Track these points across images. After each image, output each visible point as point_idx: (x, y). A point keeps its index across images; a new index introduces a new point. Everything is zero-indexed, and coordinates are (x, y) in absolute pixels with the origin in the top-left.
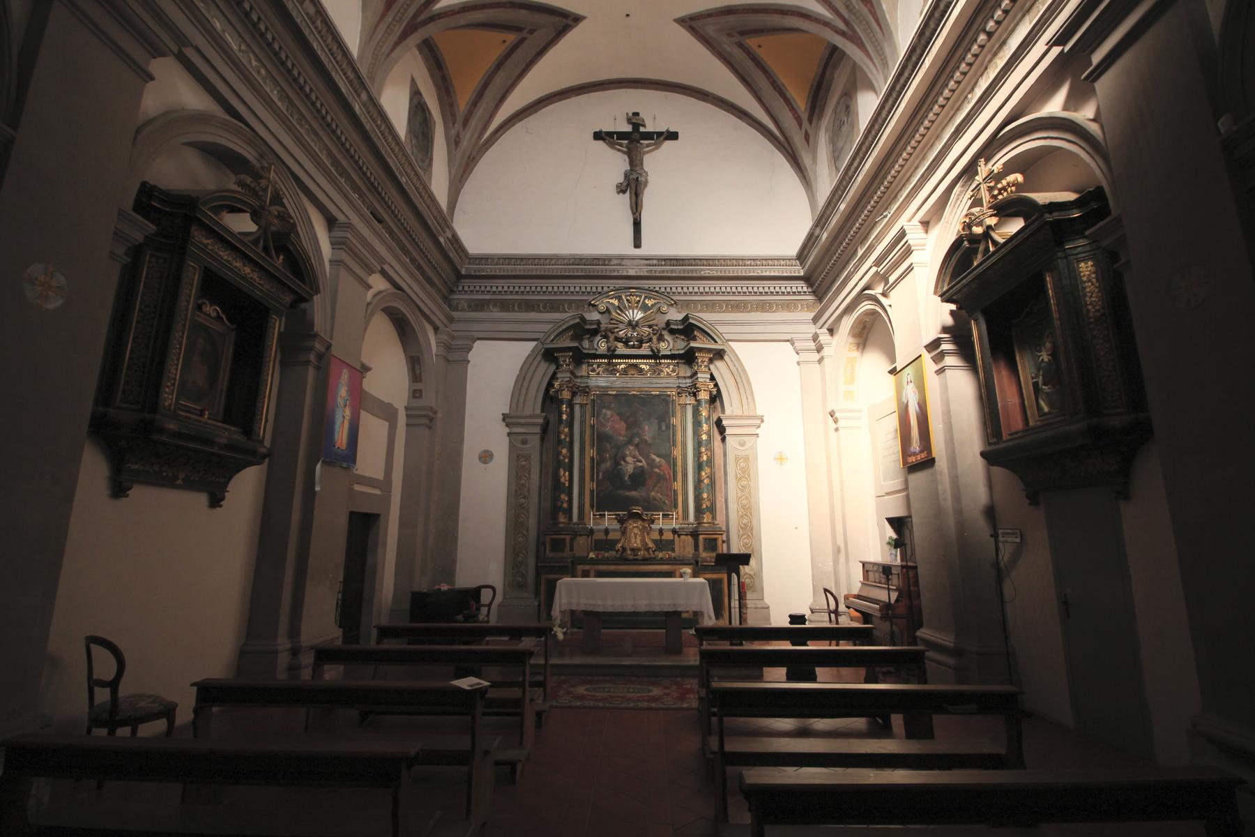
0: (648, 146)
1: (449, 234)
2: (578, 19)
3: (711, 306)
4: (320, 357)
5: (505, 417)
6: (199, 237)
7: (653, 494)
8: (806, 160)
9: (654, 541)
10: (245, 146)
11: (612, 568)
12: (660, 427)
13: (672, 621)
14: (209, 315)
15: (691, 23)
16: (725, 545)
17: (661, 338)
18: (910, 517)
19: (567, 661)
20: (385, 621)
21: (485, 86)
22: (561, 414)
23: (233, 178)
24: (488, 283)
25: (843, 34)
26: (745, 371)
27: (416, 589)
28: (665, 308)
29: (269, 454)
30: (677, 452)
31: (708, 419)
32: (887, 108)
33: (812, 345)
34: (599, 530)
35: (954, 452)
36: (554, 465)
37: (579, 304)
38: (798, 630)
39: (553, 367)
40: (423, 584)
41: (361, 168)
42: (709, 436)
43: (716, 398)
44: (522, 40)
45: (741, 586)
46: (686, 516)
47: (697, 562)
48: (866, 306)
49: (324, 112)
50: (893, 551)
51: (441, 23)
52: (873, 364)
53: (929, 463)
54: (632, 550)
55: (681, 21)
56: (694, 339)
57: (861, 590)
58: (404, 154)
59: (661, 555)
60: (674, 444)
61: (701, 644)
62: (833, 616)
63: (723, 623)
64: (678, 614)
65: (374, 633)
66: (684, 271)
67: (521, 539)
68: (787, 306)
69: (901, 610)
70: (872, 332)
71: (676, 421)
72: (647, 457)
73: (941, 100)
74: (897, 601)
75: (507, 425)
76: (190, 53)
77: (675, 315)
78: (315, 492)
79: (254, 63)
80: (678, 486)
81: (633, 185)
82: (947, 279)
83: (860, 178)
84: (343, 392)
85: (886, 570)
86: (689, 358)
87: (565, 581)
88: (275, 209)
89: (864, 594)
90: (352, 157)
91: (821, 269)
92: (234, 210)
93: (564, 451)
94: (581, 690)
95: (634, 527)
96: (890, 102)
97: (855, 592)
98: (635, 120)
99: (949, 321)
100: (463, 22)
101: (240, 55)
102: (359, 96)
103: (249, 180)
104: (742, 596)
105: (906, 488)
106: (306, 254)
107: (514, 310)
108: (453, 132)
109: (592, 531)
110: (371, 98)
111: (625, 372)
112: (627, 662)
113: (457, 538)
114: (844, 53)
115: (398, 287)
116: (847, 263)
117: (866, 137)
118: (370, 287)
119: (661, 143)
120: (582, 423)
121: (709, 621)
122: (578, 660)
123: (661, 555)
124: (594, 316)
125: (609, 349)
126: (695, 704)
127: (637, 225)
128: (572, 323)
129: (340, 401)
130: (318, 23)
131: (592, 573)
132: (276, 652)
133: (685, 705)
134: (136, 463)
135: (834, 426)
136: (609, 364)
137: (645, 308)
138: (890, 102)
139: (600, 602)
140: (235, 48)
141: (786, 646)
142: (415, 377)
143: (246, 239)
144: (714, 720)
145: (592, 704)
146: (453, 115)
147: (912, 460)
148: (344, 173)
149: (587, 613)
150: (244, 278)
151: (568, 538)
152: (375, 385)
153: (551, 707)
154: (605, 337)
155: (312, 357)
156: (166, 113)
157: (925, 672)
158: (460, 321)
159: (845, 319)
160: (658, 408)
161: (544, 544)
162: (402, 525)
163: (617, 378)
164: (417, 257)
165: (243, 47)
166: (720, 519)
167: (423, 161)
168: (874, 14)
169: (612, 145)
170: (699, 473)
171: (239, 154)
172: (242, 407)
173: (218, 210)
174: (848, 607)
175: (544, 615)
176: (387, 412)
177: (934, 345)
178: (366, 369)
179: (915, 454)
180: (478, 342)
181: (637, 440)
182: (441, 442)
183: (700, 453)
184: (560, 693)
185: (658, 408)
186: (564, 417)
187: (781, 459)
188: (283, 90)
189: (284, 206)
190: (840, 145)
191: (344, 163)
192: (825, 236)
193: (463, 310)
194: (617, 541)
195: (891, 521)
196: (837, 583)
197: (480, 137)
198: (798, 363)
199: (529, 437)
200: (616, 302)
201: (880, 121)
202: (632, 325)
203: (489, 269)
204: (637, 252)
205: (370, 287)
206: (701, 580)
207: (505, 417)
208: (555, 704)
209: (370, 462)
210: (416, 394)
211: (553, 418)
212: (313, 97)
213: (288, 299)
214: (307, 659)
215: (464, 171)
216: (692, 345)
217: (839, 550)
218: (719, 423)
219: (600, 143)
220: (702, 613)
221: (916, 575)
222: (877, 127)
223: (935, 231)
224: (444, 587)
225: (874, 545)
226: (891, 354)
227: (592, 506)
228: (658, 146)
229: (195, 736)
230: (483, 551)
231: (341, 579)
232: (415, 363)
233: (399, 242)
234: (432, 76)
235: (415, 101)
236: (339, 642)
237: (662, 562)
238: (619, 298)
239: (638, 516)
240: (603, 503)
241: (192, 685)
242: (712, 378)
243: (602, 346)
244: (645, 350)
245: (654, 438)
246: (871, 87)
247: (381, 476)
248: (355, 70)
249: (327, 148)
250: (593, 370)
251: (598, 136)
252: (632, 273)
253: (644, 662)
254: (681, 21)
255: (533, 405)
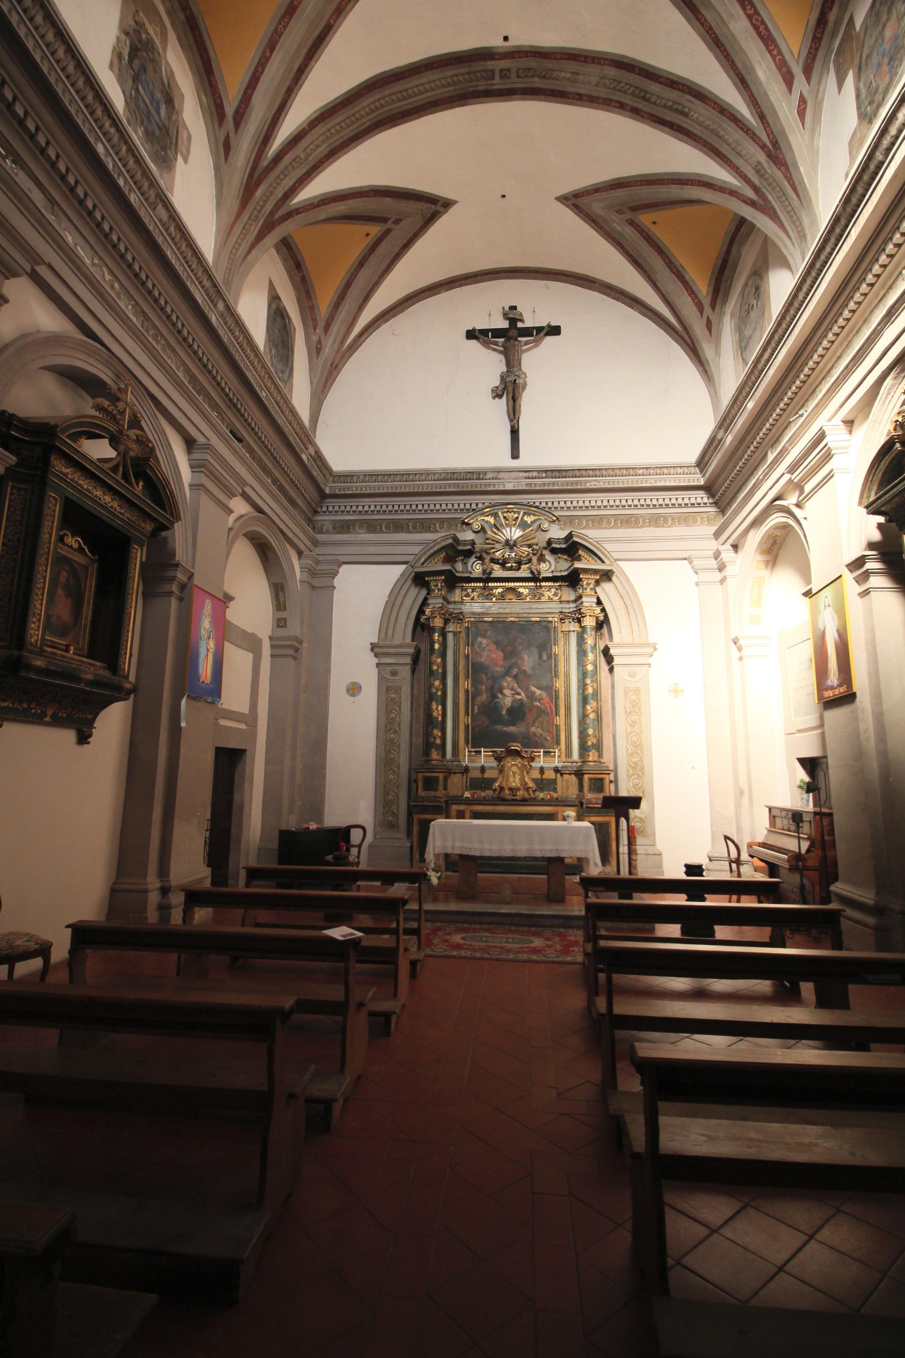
0: (526, 343)
1: (312, 451)
2: (448, 204)
3: (598, 522)
4: (183, 587)
5: (373, 647)
6: (59, 466)
7: (533, 729)
8: (708, 351)
9: (534, 780)
10: (100, 367)
11: (489, 808)
12: (540, 656)
13: (555, 866)
14: (71, 547)
15: (576, 201)
16: (612, 786)
17: (542, 559)
18: (826, 757)
19: (441, 907)
20: (253, 862)
21: (348, 285)
22: (432, 645)
23: (90, 401)
24: (353, 502)
25: (752, 204)
26: (635, 594)
27: (282, 828)
28: (546, 525)
29: (134, 690)
30: (559, 684)
31: (594, 647)
32: (805, 289)
33: (713, 563)
34: (475, 768)
35: (874, 640)
36: (427, 700)
37: (451, 522)
38: (695, 883)
39: (424, 592)
40: (292, 823)
41: (219, 384)
42: (596, 666)
43: (602, 624)
44: (389, 231)
45: (631, 831)
46: (569, 753)
47: (582, 804)
48: (777, 519)
49: (180, 325)
50: (805, 796)
51: (299, 218)
52: (784, 583)
53: (849, 698)
54: (511, 789)
55: (564, 199)
56: (579, 559)
57: (766, 837)
58: (264, 367)
59: (541, 795)
60: (556, 676)
61: (587, 896)
62: (734, 866)
63: (610, 871)
64: (560, 860)
65: (243, 874)
66: (567, 483)
67: (391, 777)
68: (685, 520)
69: (812, 862)
70: (782, 547)
71: (557, 650)
72: (527, 690)
73: (870, 278)
74: (808, 851)
75: (376, 656)
76: (43, 271)
77: (557, 533)
78: (180, 729)
79: (108, 277)
80: (560, 721)
81: (510, 389)
82: (875, 488)
83: (771, 372)
84: (206, 624)
85: (797, 817)
86: (573, 580)
87: (439, 824)
88: (133, 433)
89: (770, 842)
90: (210, 372)
91: (724, 478)
92: (92, 436)
93: (437, 683)
94: (457, 938)
95: (513, 765)
96: (809, 282)
97: (760, 839)
98: (512, 315)
99: (876, 536)
100: (323, 217)
101: (93, 269)
102: (215, 306)
103: (106, 403)
104: (631, 842)
105: (822, 725)
106: (166, 479)
107: (381, 531)
108: (315, 338)
109: (466, 770)
110: (228, 307)
111: (502, 597)
112: (505, 909)
113: (325, 774)
114: (753, 226)
115: (259, 510)
116: (756, 469)
117: (779, 324)
118: (231, 512)
119: (542, 339)
120: (456, 652)
121: (595, 869)
122: (453, 907)
123: (541, 795)
124: (468, 536)
125: (484, 572)
126: (580, 958)
127: (515, 433)
128: (444, 544)
129: (203, 633)
130: (172, 229)
131: (468, 814)
132: (146, 891)
133: (569, 959)
134: (5, 701)
135: (738, 654)
136: (484, 588)
137: (524, 525)
138: (809, 282)
139: (476, 846)
140: (88, 261)
141: (679, 900)
142: (280, 605)
143: (106, 466)
144: (602, 976)
145: (468, 954)
146: (314, 319)
147: (829, 694)
148: (201, 390)
149: (464, 857)
150: (105, 508)
151: (441, 776)
152: (236, 615)
153: (426, 956)
154: (480, 558)
155: (175, 588)
156: (23, 336)
157: (840, 934)
158: (325, 544)
159: (752, 533)
160: (539, 634)
161: (416, 781)
162: (268, 762)
163: (492, 592)
164: (279, 476)
165: (96, 261)
166: (607, 758)
167: (283, 372)
168: (790, 179)
169: (486, 344)
170: (584, 707)
171: (96, 375)
172: (106, 643)
173: (76, 437)
174: (752, 856)
175: (417, 856)
176: (251, 643)
177: (858, 563)
178: (229, 598)
179: (832, 688)
180: (344, 566)
181: (515, 671)
182: (304, 674)
183: (585, 685)
184: (436, 941)
185: (539, 634)
186: (437, 646)
187: (676, 691)
188: (137, 304)
189: (142, 429)
190: (747, 333)
191: (201, 378)
192: (729, 439)
193: (328, 532)
194: (494, 780)
195: (803, 762)
196: (739, 829)
197: (342, 342)
198: (697, 584)
199: (398, 668)
200: (492, 520)
201: (796, 304)
202: (510, 545)
203: (354, 487)
204: (515, 463)
205: (231, 512)
206: (586, 824)
207: (373, 647)
208: (429, 952)
209: (235, 695)
210: (280, 623)
211: (424, 647)
212: (169, 310)
213: (149, 527)
214: (177, 899)
215: (327, 381)
216: (575, 565)
217: (741, 793)
218: (606, 652)
219: (474, 342)
220: (587, 860)
221: (832, 823)
222: (792, 312)
223: (861, 431)
224: (313, 826)
225: (786, 789)
226: (805, 572)
227: (467, 743)
228: (537, 343)
229: (71, 980)
230: (352, 794)
231: (209, 817)
232: (278, 590)
233: (260, 462)
234: (292, 279)
235: (274, 306)
236: (207, 884)
237: (543, 802)
238: (496, 515)
239: (517, 753)
240: (478, 740)
241: (67, 927)
242: (599, 602)
243: (477, 569)
244: (524, 572)
245: (533, 669)
246: (785, 264)
247: (245, 710)
248: (210, 278)
249: (184, 363)
250: (468, 595)
251: (471, 335)
252: (509, 487)
253: (524, 910)
254: (564, 199)
255: (403, 634)
